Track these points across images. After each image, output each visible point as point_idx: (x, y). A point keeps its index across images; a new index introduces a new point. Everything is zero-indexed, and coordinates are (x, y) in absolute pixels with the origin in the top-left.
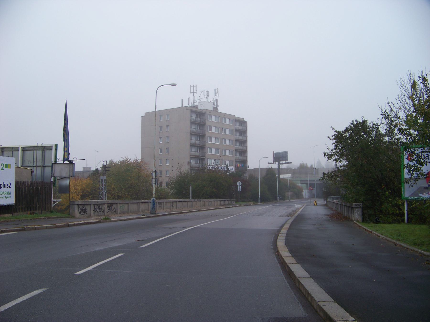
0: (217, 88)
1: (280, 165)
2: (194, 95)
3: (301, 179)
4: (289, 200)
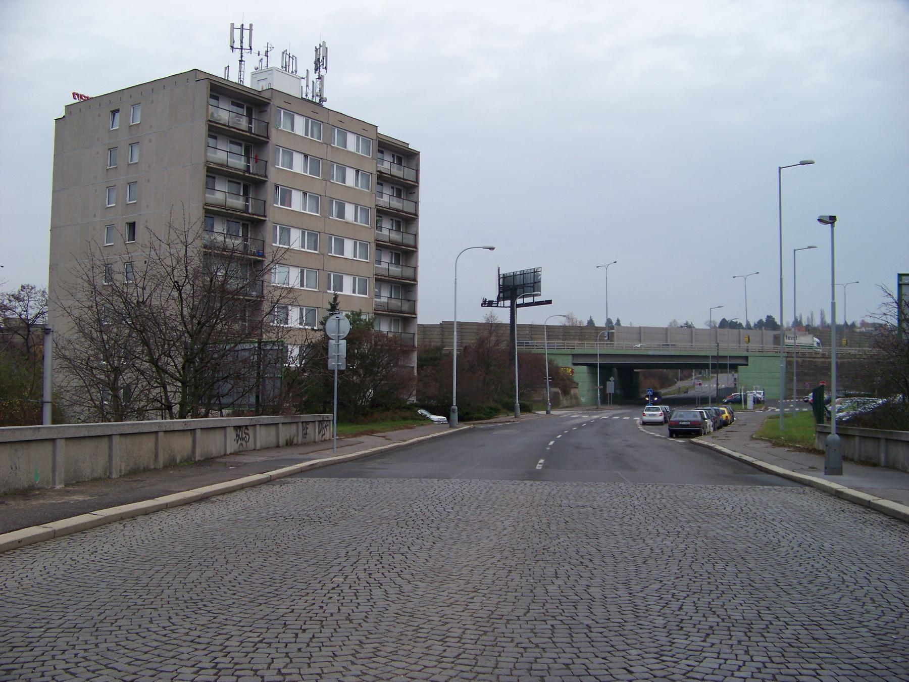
0: (324, 42)
1: (519, 311)
2: (242, 56)
3: (574, 352)
4: (548, 413)
